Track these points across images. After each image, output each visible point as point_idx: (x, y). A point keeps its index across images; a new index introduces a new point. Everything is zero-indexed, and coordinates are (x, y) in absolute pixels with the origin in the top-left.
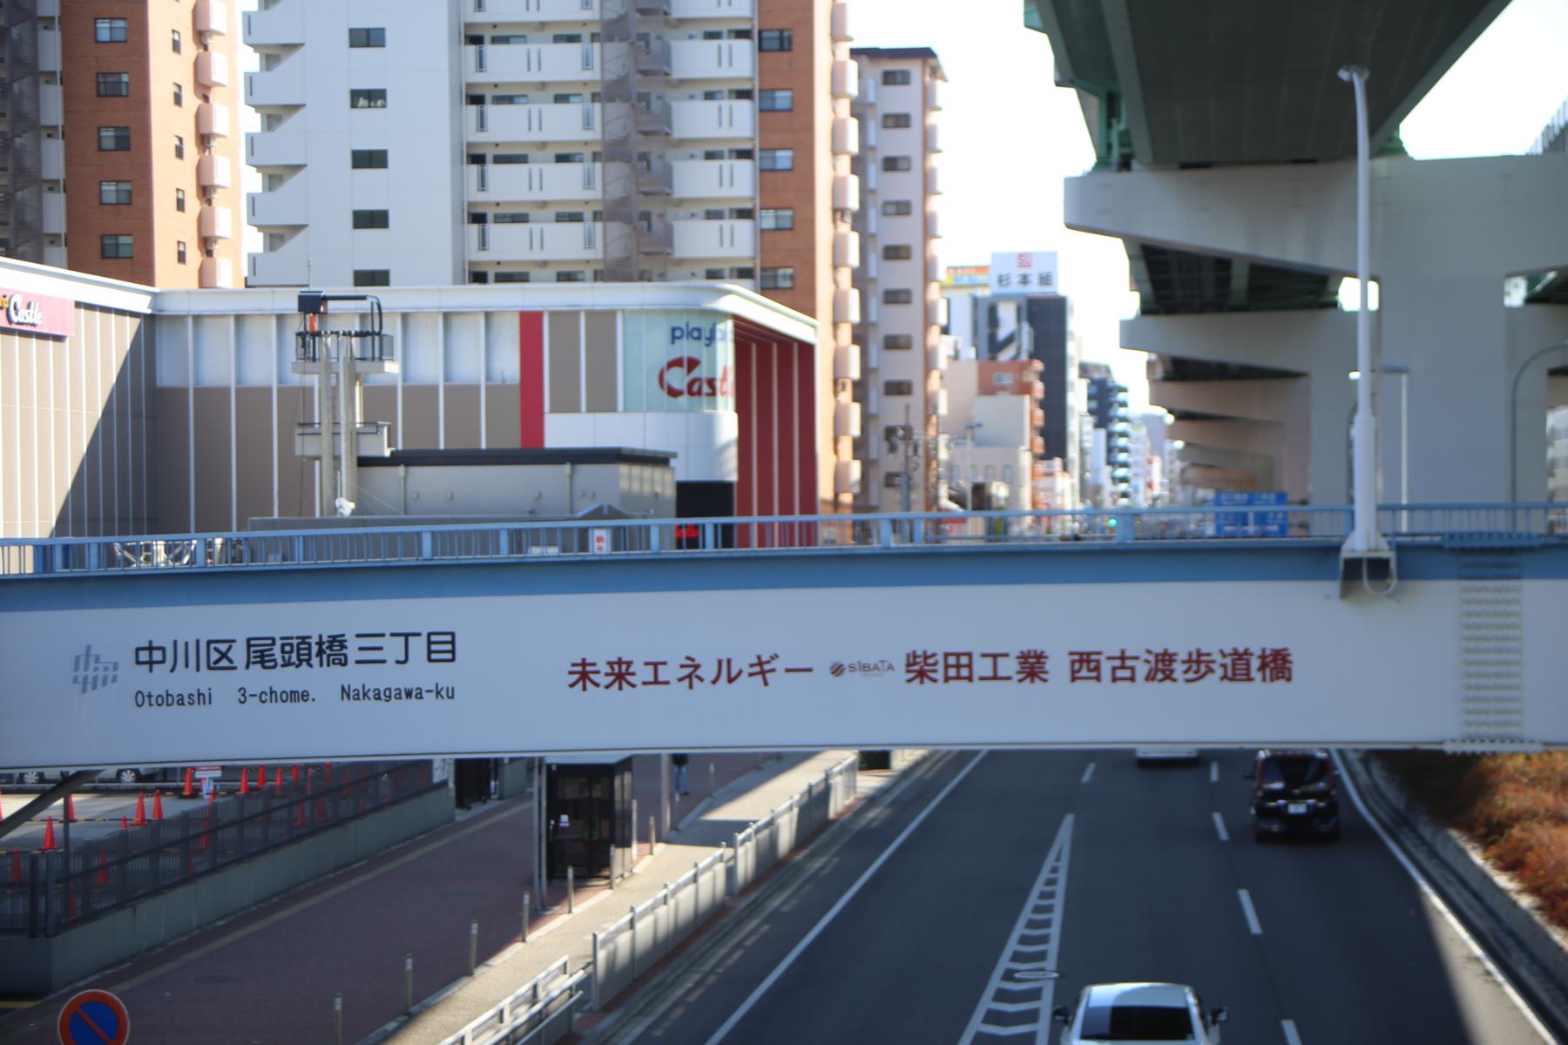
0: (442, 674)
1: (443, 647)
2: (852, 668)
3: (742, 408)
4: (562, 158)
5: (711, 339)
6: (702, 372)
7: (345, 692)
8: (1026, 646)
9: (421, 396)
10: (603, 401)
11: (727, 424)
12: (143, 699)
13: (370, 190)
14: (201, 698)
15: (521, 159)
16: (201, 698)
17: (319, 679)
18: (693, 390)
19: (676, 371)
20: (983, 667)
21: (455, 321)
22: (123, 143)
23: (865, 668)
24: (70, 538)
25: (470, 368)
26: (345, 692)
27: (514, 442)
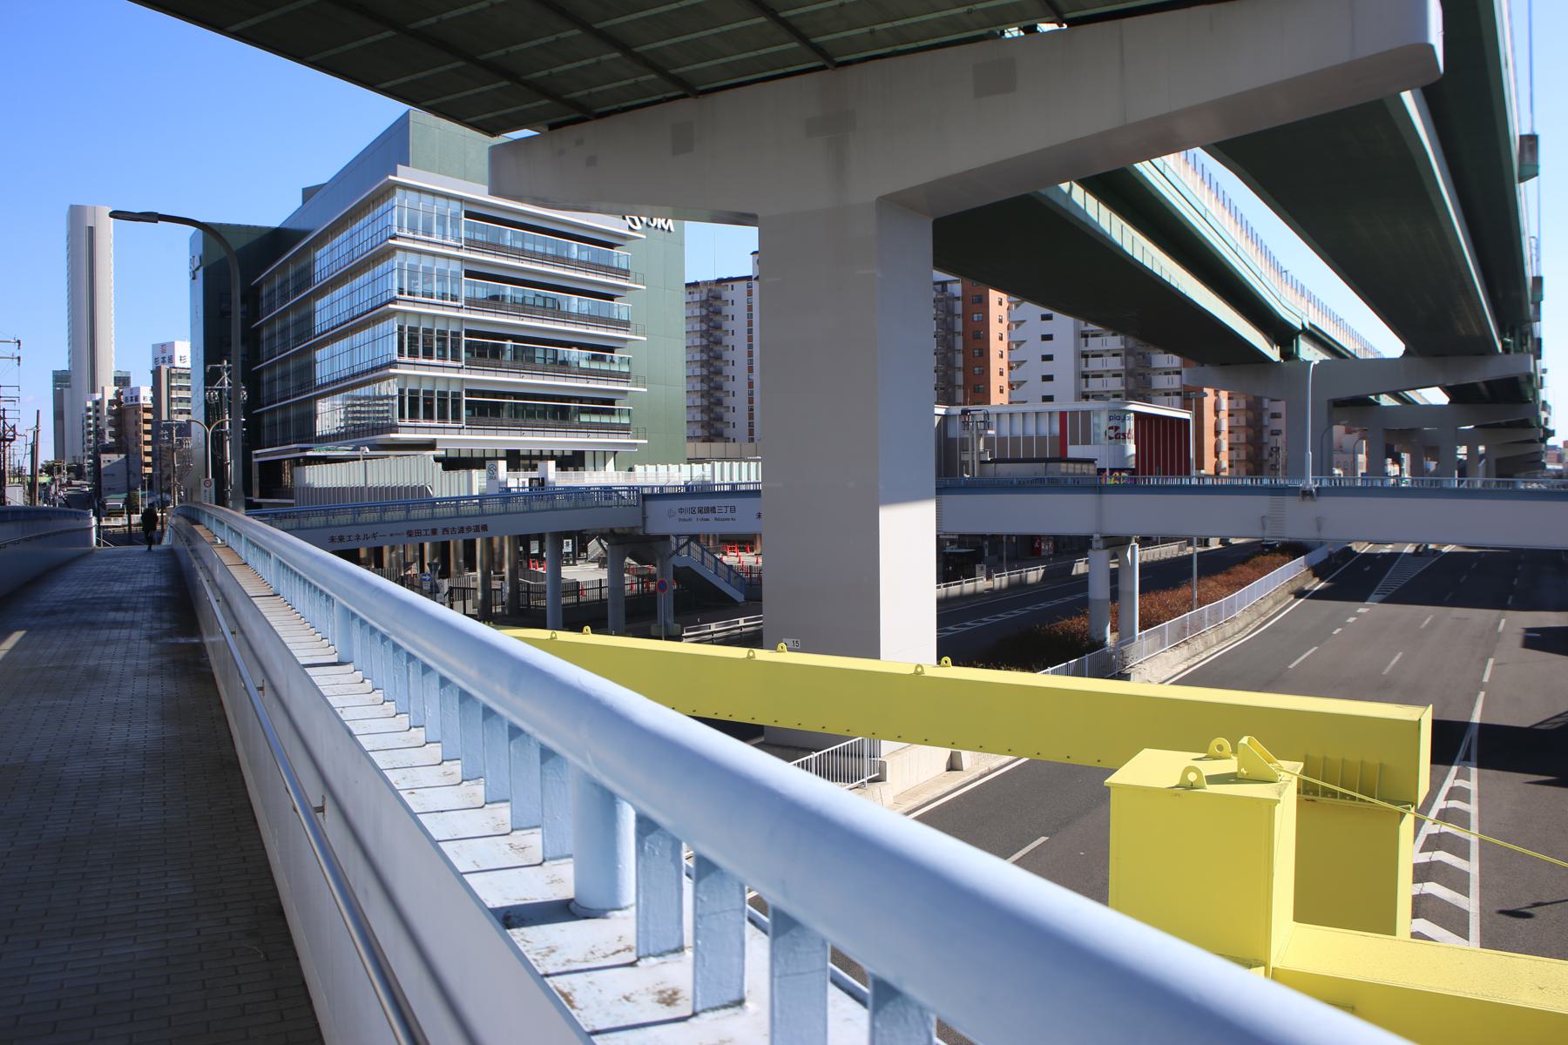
0: (733, 515)
1: (733, 509)
2: (396, 534)
3: (1136, 443)
4: (1114, 355)
5: (1124, 419)
6: (1121, 431)
7: (716, 519)
8: (433, 527)
9: (1002, 440)
10: (1086, 441)
11: (1131, 448)
12: (680, 520)
13: (1048, 368)
14: (690, 520)
15: (1101, 356)
16: (690, 520)
17: (710, 516)
18: (1117, 437)
19: (1111, 431)
20: (424, 533)
21: (1040, 415)
22: (981, 354)
23: (398, 534)
24: (478, 484)
25: (1045, 430)
26: (716, 519)
27: (1058, 455)
